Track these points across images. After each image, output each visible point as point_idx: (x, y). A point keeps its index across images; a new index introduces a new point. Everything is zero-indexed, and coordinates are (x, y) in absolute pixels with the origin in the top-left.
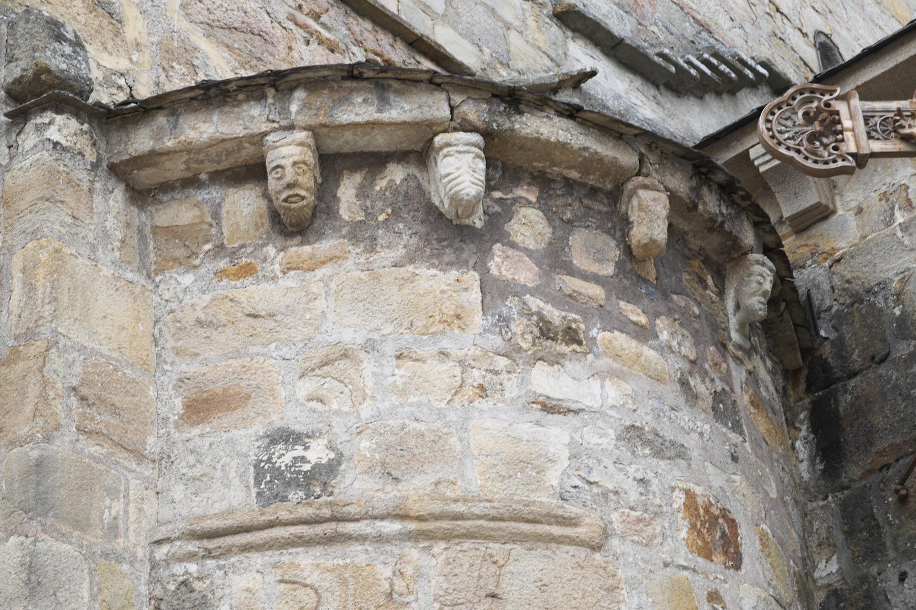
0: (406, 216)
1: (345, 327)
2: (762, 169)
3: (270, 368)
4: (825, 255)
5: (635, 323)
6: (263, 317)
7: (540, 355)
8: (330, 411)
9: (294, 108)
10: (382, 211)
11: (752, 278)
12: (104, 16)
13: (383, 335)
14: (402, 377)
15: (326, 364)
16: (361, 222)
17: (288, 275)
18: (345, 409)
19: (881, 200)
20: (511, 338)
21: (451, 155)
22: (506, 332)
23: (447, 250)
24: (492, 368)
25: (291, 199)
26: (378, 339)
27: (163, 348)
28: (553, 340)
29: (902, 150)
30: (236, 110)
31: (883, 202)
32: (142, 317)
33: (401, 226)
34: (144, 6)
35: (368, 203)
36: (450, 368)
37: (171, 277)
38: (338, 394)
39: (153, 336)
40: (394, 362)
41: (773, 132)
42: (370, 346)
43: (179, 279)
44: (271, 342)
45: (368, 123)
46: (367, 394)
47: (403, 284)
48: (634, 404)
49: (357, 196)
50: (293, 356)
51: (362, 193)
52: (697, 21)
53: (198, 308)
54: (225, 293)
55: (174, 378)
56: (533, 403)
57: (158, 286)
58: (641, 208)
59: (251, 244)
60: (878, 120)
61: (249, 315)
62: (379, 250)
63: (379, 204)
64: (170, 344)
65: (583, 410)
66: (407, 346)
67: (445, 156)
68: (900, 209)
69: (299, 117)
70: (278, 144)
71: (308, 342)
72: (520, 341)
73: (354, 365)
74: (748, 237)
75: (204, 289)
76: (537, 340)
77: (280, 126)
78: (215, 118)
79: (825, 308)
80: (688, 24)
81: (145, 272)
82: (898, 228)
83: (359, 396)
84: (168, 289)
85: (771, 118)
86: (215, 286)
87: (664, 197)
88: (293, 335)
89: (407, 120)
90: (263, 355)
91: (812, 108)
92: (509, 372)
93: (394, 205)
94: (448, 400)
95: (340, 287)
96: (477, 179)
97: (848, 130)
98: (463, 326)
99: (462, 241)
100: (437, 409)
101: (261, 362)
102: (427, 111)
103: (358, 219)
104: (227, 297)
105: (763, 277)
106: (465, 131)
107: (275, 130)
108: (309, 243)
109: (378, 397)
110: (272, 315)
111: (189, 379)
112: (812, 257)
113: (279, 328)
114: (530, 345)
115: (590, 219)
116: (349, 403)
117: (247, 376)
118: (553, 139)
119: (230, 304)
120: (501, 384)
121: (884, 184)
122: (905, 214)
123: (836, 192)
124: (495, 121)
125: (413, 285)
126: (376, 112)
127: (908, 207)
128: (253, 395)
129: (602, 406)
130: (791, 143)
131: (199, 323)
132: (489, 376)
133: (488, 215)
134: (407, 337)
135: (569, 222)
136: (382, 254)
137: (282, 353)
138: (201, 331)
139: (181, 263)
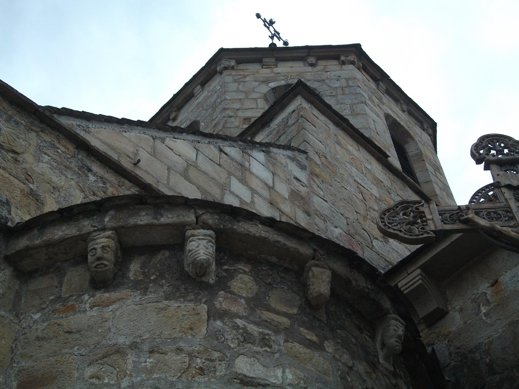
0: (167, 276)
1: (121, 336)
2: (405, 292)
3: (72, 361)
4: (444, 336)
5: (309, 340)
6: (74, 333)
7: (242, 351)
8: (102, 384)
9: (107, 219)
10: (153, 274)
11: (391, 327)
12: (33, 200)
13: (143, 339)
14: (150, 363)
15: (106, 357)
16: (140, 280)
17: (93, 309)
18: (112, 382)
19: (472, 302)
20: (224, 341)
21: (194, 241)
22: (221, 338)
23: (190, 294)
24: (209, 358)
25: (99, 266)
26: (140, 341)
27: (15, 354)
28: (252, 344)
29: (463, 228)
30: (76, 223)
31: (474, 304)
32: (6, 336)
33: (164, 281)
34: (59, 199)
35: (146, 270)
36: (183, 358)
37: (29, 316)
38: (109, 374)
39: (12, 348)
40: (148, 355)
41: (385, 223)
42: (134, 346)
43: (33, 316)
44: (76, 346)
45: (147, 225)
46: (127, 373)
47: (160, 312)
48: (305, 384)
49: (141, 267)
50: (87, 353)
51: (143, 266)
52: (387, 261)
53: (39, 330)
54: (55, 321)
55: (17, 370)
56: (235, 379)
57: (21, 321)
58: (314, 277)
59: (75, 295)
60: (448, 215)
61: (67, 332)
62: (148, 294)
63: (153, 270)
64: (20, 351)
65: (269, 385)
66: (157, 346)
67: (191, 241)
68: (483, 305)
69: (108, 224)
70: (95, 238)
71: (97, 345)
72: (229, 343)
73: (123, 357)
74: (387, 304)
75: (44, 320)
76: (241, 343)
77: (98, 229)
78: (64, 228)
79: (447, 364)
80: (382, 261)
81: (14, 313)
82: (483, 316)
83: (122, 374)
84: (26, 322)
85: (383, 216)
86: (51, 318)
87: (328, 273)
88: (89, 341)
89: (169, 222)
90: (70, 353)
91: (408, 211)
92: (220, 360)
93: (161, 271)
94: (178, 376)
95: (121, 314)
96: (208, 252)
97: (429, 220)
98: (194, 334)
99: (200, 289)
100: (171, 381)
101: (67, 358)
102: (181, 218)
103: (140, 278)
104: (56, 323)
105: (397, 327)
106: (204, 228)
107: (95, 231)
108: (108, 292)
109: (134, 375)
110: (79, 331)
111: (24, 370)
112: (438, 339)
113: (81, 338)
114: (236, 345)
115: (284, 284)
116: (115, 379)
117: (57, 366)
118: (257, 235)
119: (57, 327)
120: (214, 367)
121: (473, 294)
122: (486, 307)
123: (448, 303)
124: (222, 224)
125: (166, 312)
126: (152, 219)
127: (488, 304)
128: (58, 377)
129: (282, 383)
130: (396, 228)
131: (38, 338)
132: (207, 362)
133: (219, 277)
134: (158, 340)
135: (270, 284)
136: (150, 296)
137: (80, 352)
138: (37, 343)
139: (36, 307)
